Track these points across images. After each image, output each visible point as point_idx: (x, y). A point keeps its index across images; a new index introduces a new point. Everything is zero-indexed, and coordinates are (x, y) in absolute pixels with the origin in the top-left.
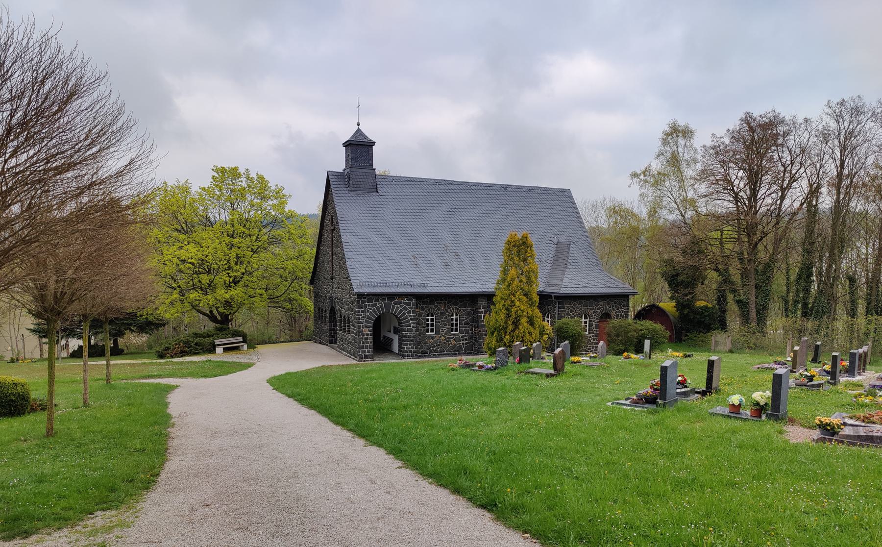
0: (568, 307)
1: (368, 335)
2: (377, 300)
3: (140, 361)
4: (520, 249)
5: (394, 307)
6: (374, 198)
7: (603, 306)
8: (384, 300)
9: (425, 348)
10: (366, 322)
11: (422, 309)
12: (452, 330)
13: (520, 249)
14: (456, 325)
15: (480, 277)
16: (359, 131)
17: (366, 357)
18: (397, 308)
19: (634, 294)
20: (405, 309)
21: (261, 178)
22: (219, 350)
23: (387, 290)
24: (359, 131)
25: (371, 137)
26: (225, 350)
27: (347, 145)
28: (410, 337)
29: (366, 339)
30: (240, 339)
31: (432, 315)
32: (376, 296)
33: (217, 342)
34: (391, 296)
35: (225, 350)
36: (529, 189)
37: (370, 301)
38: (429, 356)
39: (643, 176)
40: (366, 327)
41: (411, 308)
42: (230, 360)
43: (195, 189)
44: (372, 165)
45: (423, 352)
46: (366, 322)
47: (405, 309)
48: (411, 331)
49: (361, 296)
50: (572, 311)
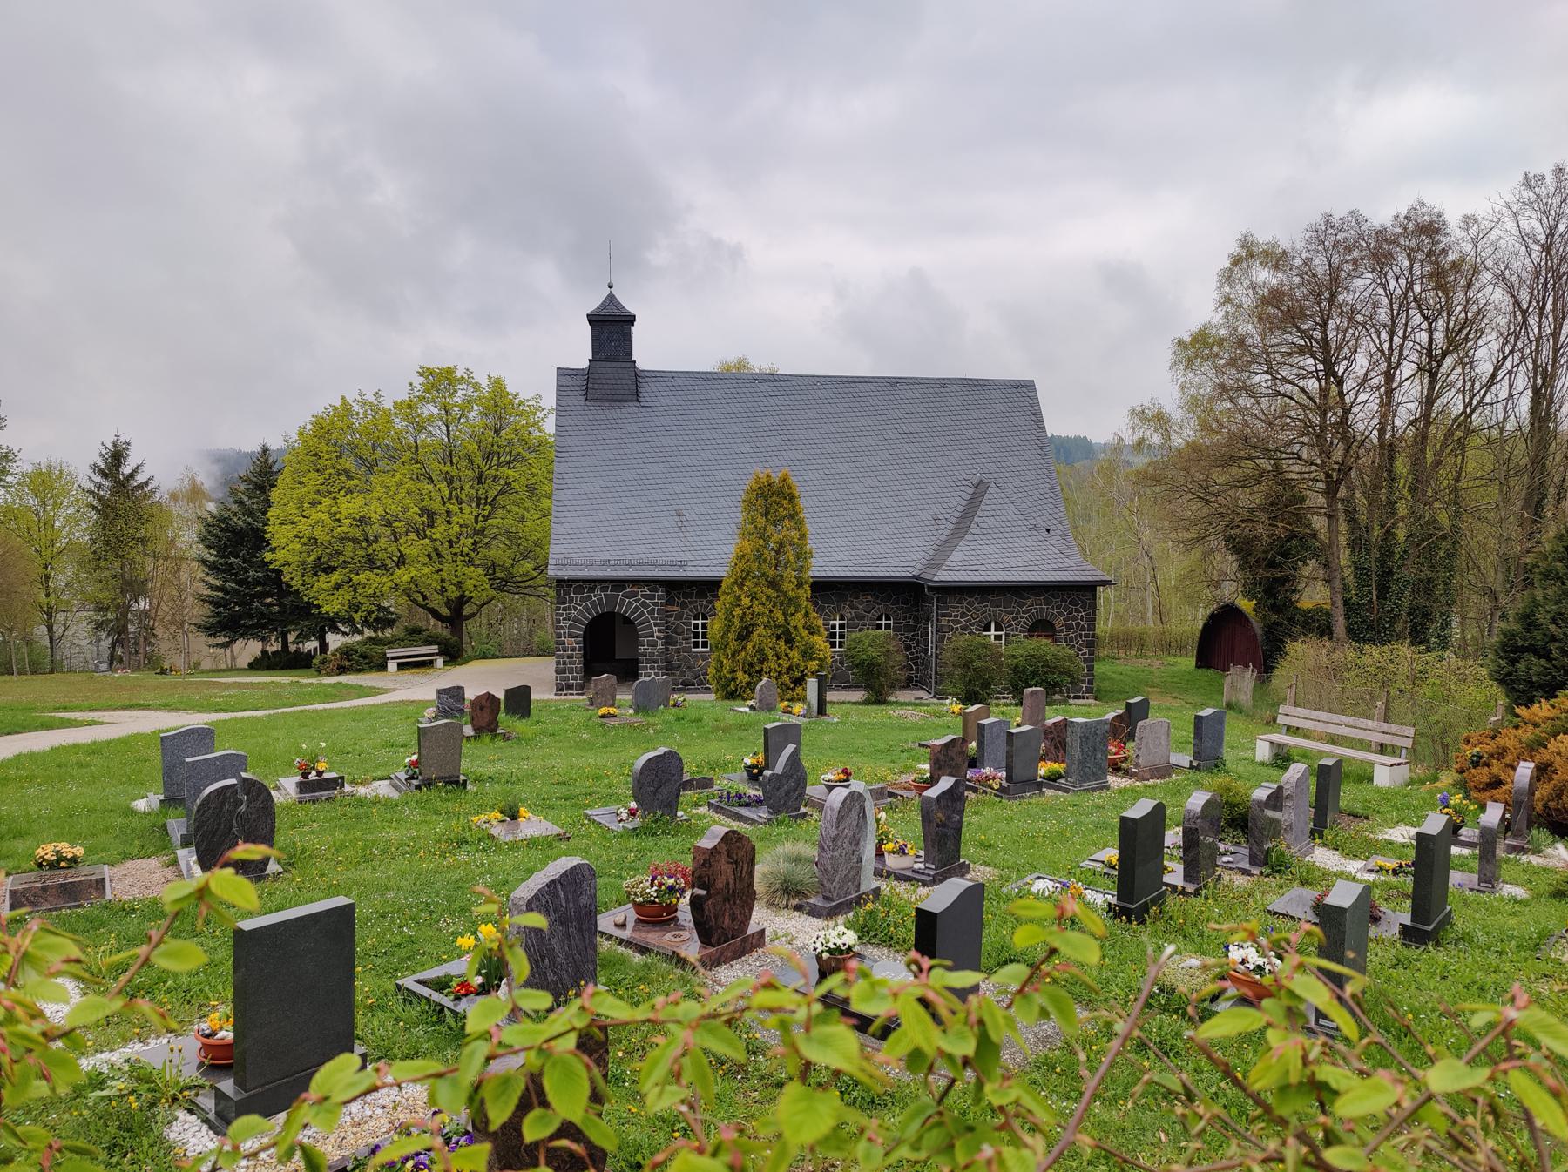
0: (956, 608)
1: (573, 649)
2: (592, 590)
3: (268, 679)
4: (773, 502)
5: (623, 602)
6: (630, 412)
7: (1036, 607)
8: (604, 589)
9: (688, 676)
10: (571, 627)
11: (684, 606)
12: (696, 645)
13: (773, 502)
14: (704, 635)
15: (711, 550)
16: (611, 296)
17: (570, 687)
18: (627, 605)
19: (1105, 583)
20: (644, 605)
21: (498, 384)
22: (392, 666)
23: (609, 572)
24: (611, 296)
25: (630, 307)
26: (401, 666)
27: (593, 320)
28: (652, 655)
29: (570, 657)
30: (434, 649)
31: (704, 617)
32: (593, 583)
33: (390, 652)
34: (619, 584)
35: (401, 666)
36: (944, 383)
37: (579, 590)
38: (696, 691)
39: (1197, 348)
40: (571, 636)
41: (656, 604)
42: (369, 684)
43: (1170, 400)
44: (630, 354)
45: (685, 684)
46: (571, 627)
47: (644, 605)
48: (654, 644)
49: (561, 583)
50: (963, 615)
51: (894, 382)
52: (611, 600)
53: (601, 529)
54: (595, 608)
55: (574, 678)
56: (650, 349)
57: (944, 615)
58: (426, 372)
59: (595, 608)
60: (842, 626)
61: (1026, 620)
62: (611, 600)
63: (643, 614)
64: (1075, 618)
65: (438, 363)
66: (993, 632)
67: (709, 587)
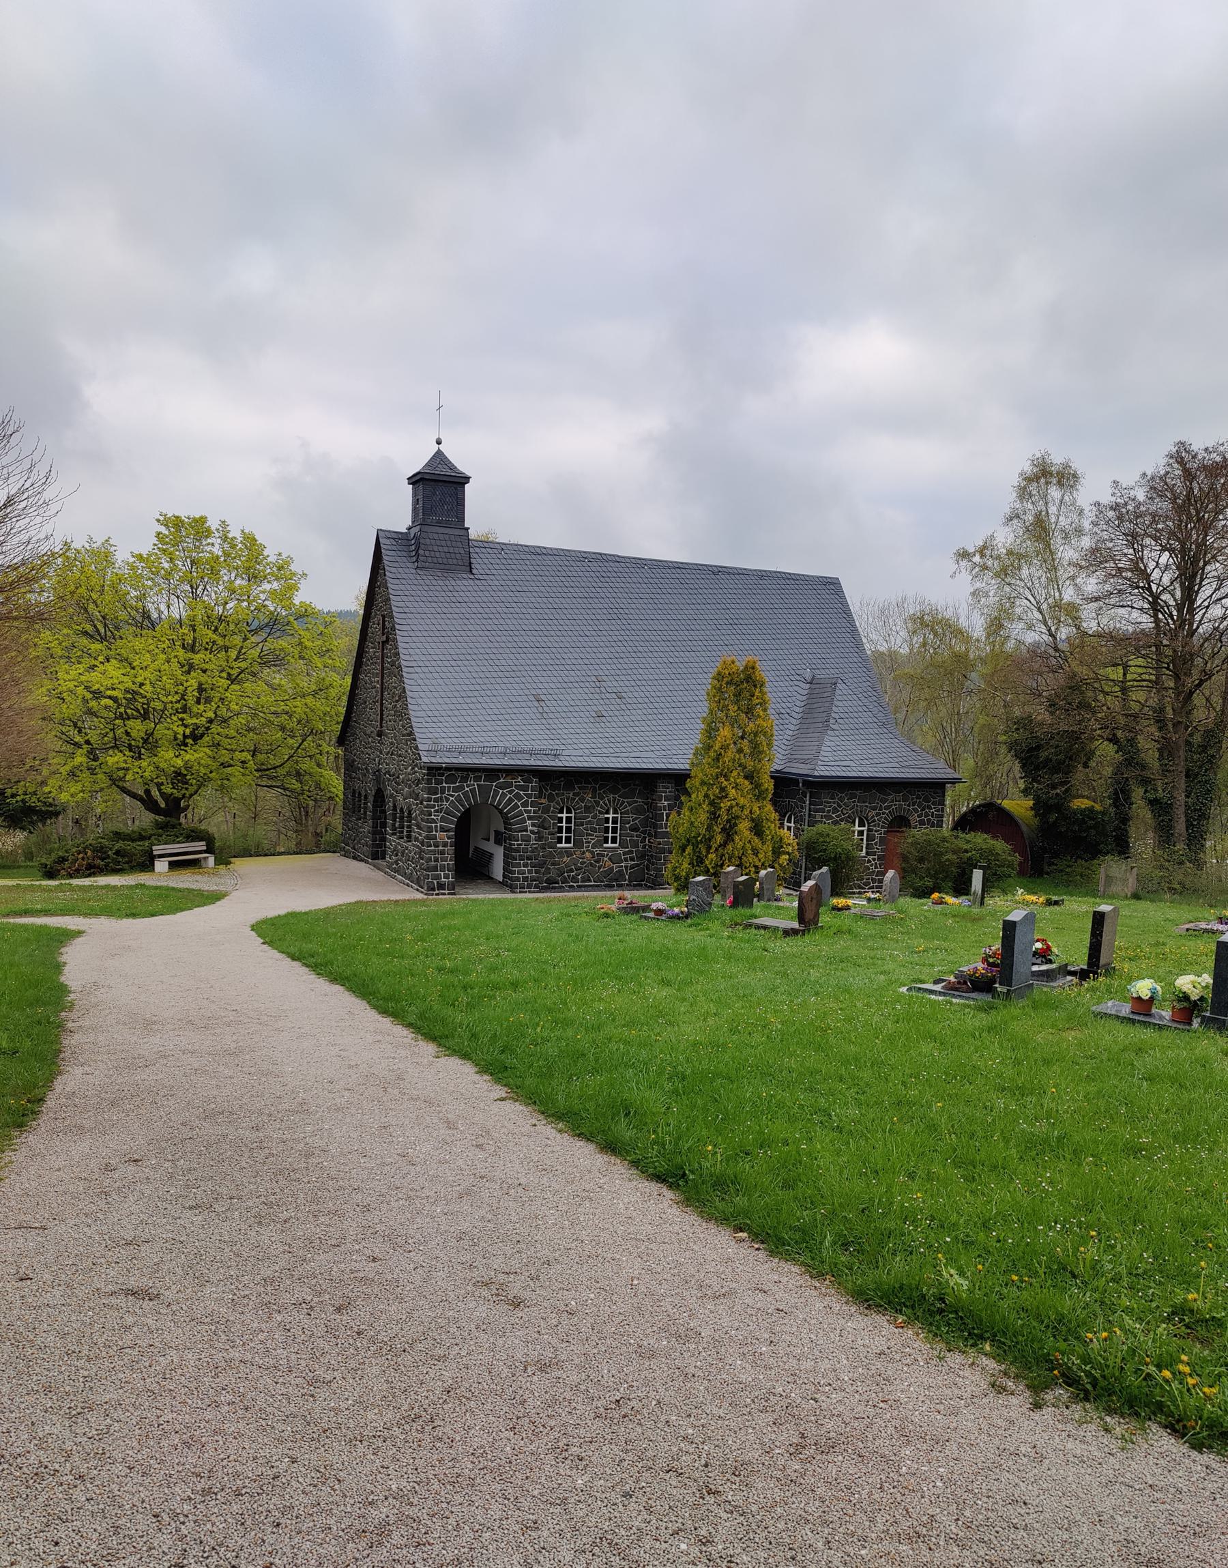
1: (445, 845)
4: (739, 690)
5: (496, 793)
6: (464, 585)
7: (895, 803)
8: (477, 779)
9: (553, 874)
10: (443, 819)
13: (739, 690)
15: (662, 739)
16: (439, 454)
17: (441, 886)
18: (502, 796)
19: (954, 781)
20: (518, 797)
21: (250, 540)
22: (161, 866)
24: (439, 454)
26: (173, 865)
28: (525, 851)
29: (442, 853)
30: (202, 845)
31: (569, 811)
33: (158, 849)
34: (492, 773)
35: (173, 865)
37: (451, 779)
38: (561, 889)
40: (443, 829)
41: (529, 796)
45: (549, 881)
46: (443, 819)
47: (518, 797)
48: (527, 839)
49: (434, 771)
51: (716, 571)
52: (484, 791)
53: (462, 712)
54: (468, 800)
55: (446, 877)
56: (482, 515)
57: (818, 811)
58: (166, 521)
59: (468, 800)
60: (569, 820)
61: (886, 816)
62: (484, 791)
63: (516, 806)
64: (927, 815)
65: (186, 511)
66: (857, 828)
67: (679, 779)
